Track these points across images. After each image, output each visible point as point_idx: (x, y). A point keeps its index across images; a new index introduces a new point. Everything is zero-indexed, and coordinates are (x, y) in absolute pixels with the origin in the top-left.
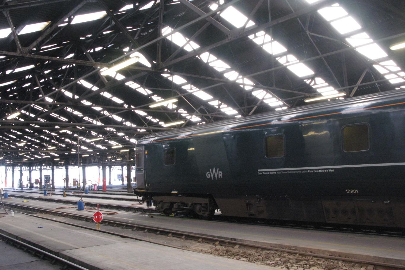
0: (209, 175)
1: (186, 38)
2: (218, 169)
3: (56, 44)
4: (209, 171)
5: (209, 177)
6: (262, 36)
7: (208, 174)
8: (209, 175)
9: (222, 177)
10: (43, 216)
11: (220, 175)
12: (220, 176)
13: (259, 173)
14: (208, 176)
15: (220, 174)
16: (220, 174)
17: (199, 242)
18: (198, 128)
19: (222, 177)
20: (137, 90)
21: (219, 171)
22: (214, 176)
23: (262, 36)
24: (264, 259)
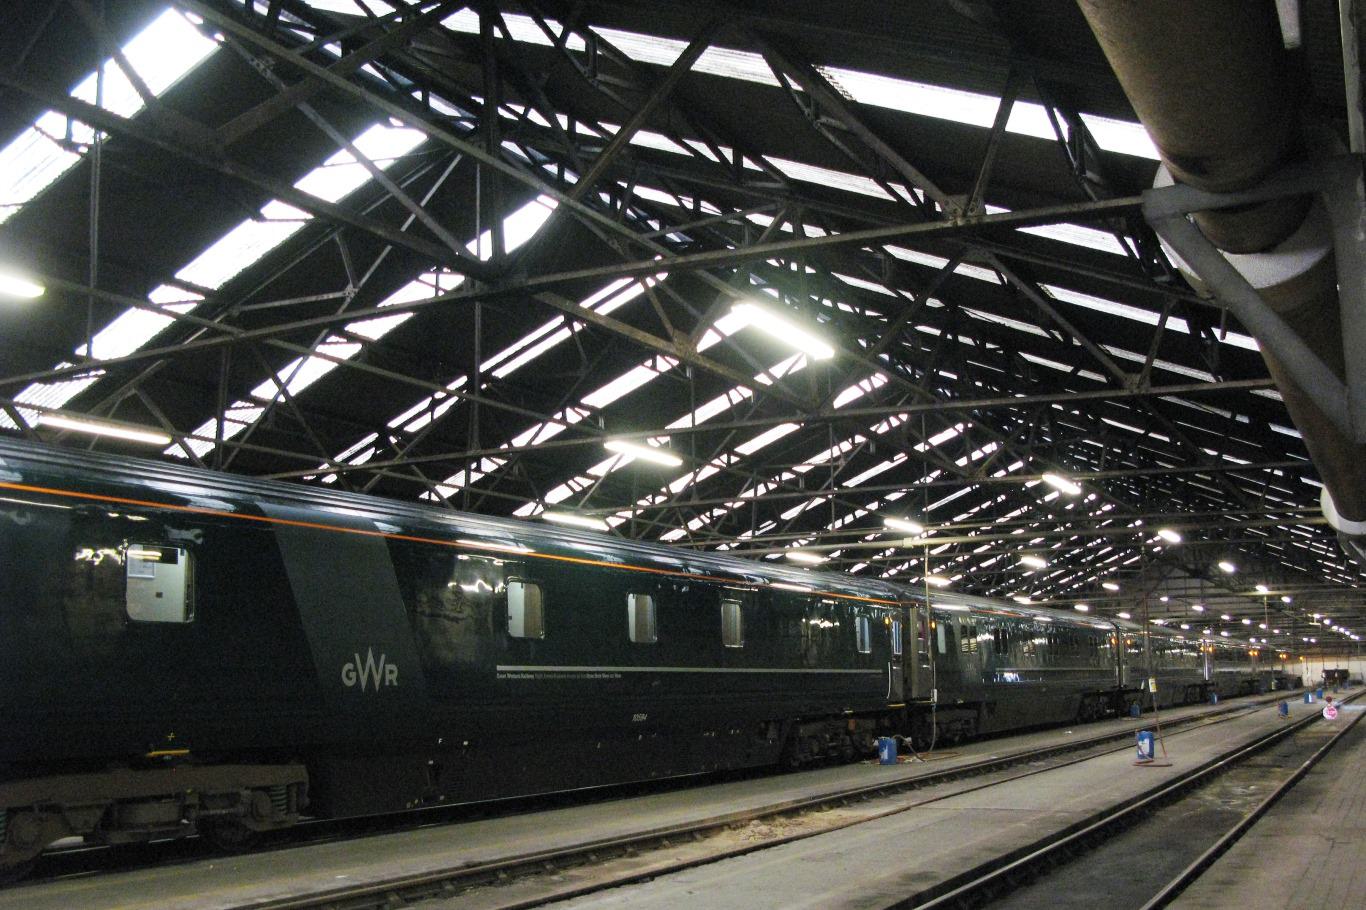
0: (353, 675)
1: (189, 15)
2: (383, 657)
3: (1138, 257)
4: (353, 661)
5: (350, 683)
6: (424, 282)
7: (349, 670)
8: (353, 675)
9: (395, 684)
10: (584, 876)
11: (388, 677)
12: (391, 681)
13: (499, 676)
14: (350, 679)
15: (391, 672)
16: (391, 672)
17: (503, 883)
18: (55, 456)
19: (395, 684)
20: (94, 76)
21: (387, 662)
22: (370, 676)
23: (424, 282)
24: (1146, 706)
